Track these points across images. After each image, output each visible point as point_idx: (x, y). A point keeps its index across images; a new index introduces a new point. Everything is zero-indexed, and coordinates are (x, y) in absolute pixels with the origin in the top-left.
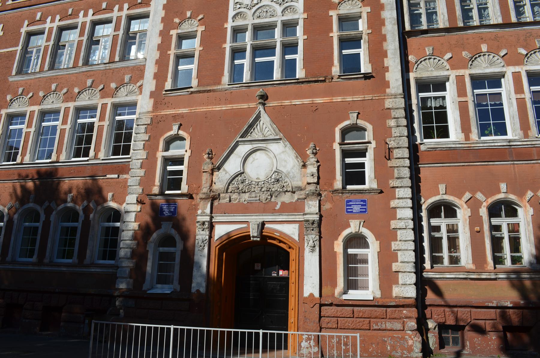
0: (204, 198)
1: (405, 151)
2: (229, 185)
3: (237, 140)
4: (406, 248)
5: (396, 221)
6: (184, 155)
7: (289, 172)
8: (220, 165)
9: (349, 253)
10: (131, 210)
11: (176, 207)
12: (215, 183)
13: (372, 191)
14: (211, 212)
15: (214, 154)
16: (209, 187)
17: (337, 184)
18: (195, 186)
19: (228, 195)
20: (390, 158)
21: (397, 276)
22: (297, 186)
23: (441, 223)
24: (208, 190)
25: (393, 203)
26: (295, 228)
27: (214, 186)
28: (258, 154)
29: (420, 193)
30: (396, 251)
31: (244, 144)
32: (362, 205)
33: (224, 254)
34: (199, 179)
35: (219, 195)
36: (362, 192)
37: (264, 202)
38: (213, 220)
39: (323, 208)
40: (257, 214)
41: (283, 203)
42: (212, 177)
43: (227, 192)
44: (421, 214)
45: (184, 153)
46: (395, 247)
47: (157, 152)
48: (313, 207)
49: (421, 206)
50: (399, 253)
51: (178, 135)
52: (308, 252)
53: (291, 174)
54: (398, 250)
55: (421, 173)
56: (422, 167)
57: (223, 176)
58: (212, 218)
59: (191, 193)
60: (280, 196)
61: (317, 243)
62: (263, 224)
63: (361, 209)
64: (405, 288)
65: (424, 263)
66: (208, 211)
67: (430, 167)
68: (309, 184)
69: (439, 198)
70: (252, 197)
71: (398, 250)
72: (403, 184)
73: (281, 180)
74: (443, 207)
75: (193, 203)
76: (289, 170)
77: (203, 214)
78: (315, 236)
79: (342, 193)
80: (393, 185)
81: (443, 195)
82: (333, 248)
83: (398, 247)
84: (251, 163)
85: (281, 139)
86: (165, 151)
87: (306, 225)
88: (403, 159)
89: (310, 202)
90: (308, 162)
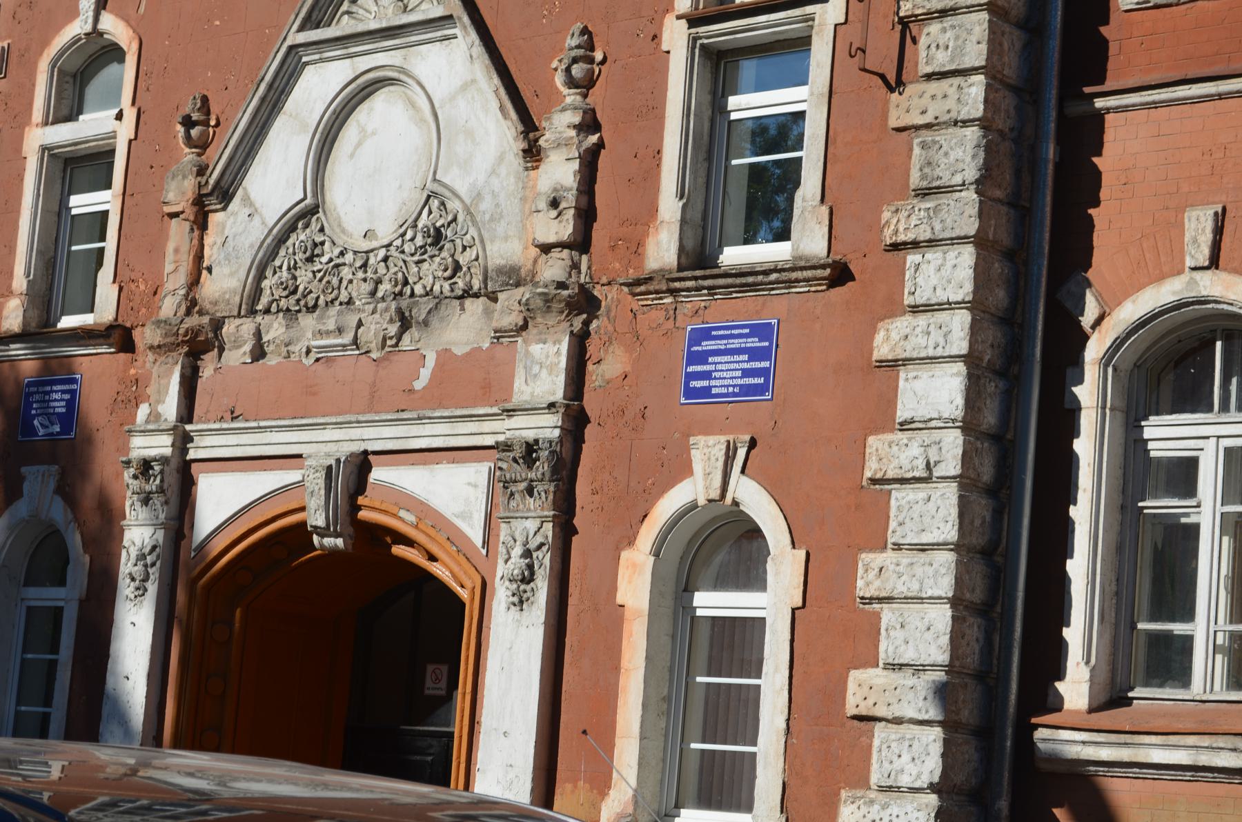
0: (159, 346)
1: (970, 32)
2: (261, 276)
3: (289, 42)
4: (914, 588)
5: (889, 437)
6: (113, 135)
7: (479, 194)
8: (228, 178)
9: (699, 613)
10: (907, 355)
11: (73, 392)
12: (209, 270)
13: (794, 275)
14: (187, 411)
15: (598, 56)
16: (183, 292)
17: (658, 244)
18: (142, 287)
19: (248, 326)
20: (904, 78)
21: (863, 739)
22: (503, 262)
23: (1200, 444)
24: (179, 306)
25: (885, 343)
26: (476, 486)
27: (208, 282)
28: (380, 106)
29: (1088, 265)
30: (876, 606)
31: (322, 60)
32: (754, 354)
33: (238, 611)
34: (156, 249)
35: (218, 325)
36: (750, 279)
37: (374, 355)
38: (192, 455)
39: (596, 375)
40: (348, 418)
41: (445, 356)
42: (201, 239)
43: (252, 312)
44: (1075, 389)
45: (112, 125)
46: (868, 584)
47: (27, 129)
48: (544, 373)
49: (1082, 339)
50: (888, 615)
51: (101, 34)
52: (503, 606)
53: (486, 205)
54: (881, 600)
55: (1107, 149)
56: (1125, 109)
57: (240, 230)
58: (183, 440)
59: (128, 325)
60: (442, 319)
61: (544, 560)
62: (362, 464)
63: (747, 373)
64: (885, 807)
65: (1060, 674)
66: (170, 408)
67: (1154, 105)
68: (546, 249)
69: (1174, 293)
70: (328, 333)
71: (881, 600)
72: (938, 227)
73: (449, 233)
74: (1219, 344)
75: (132, 371)
76: (482, 178)
77: (154, 426)
78: (537, 523)
79: (673, 292)
80: (896, 232)
81: (1198, 275)
82: (614, 589)
83: (877, 583)
84: (352, 156)
85: (450, 17)
86: (58, 120)
87: (504, 466)
88: (956, 81)
89: (536, 349)
90: (548, 135)
